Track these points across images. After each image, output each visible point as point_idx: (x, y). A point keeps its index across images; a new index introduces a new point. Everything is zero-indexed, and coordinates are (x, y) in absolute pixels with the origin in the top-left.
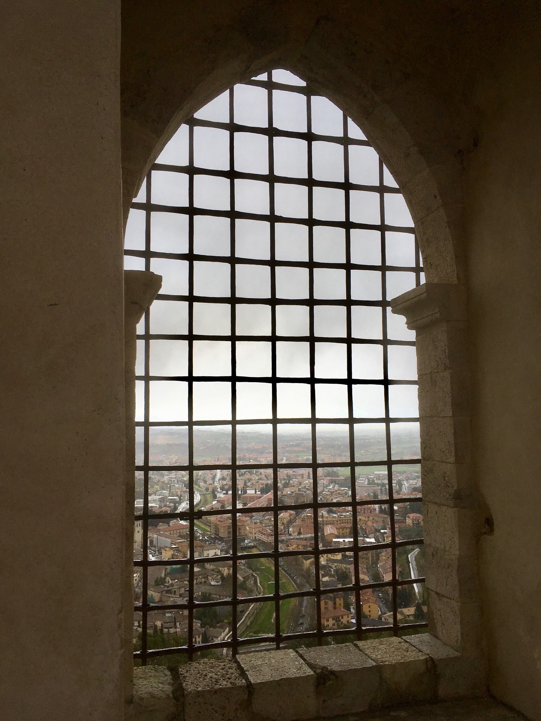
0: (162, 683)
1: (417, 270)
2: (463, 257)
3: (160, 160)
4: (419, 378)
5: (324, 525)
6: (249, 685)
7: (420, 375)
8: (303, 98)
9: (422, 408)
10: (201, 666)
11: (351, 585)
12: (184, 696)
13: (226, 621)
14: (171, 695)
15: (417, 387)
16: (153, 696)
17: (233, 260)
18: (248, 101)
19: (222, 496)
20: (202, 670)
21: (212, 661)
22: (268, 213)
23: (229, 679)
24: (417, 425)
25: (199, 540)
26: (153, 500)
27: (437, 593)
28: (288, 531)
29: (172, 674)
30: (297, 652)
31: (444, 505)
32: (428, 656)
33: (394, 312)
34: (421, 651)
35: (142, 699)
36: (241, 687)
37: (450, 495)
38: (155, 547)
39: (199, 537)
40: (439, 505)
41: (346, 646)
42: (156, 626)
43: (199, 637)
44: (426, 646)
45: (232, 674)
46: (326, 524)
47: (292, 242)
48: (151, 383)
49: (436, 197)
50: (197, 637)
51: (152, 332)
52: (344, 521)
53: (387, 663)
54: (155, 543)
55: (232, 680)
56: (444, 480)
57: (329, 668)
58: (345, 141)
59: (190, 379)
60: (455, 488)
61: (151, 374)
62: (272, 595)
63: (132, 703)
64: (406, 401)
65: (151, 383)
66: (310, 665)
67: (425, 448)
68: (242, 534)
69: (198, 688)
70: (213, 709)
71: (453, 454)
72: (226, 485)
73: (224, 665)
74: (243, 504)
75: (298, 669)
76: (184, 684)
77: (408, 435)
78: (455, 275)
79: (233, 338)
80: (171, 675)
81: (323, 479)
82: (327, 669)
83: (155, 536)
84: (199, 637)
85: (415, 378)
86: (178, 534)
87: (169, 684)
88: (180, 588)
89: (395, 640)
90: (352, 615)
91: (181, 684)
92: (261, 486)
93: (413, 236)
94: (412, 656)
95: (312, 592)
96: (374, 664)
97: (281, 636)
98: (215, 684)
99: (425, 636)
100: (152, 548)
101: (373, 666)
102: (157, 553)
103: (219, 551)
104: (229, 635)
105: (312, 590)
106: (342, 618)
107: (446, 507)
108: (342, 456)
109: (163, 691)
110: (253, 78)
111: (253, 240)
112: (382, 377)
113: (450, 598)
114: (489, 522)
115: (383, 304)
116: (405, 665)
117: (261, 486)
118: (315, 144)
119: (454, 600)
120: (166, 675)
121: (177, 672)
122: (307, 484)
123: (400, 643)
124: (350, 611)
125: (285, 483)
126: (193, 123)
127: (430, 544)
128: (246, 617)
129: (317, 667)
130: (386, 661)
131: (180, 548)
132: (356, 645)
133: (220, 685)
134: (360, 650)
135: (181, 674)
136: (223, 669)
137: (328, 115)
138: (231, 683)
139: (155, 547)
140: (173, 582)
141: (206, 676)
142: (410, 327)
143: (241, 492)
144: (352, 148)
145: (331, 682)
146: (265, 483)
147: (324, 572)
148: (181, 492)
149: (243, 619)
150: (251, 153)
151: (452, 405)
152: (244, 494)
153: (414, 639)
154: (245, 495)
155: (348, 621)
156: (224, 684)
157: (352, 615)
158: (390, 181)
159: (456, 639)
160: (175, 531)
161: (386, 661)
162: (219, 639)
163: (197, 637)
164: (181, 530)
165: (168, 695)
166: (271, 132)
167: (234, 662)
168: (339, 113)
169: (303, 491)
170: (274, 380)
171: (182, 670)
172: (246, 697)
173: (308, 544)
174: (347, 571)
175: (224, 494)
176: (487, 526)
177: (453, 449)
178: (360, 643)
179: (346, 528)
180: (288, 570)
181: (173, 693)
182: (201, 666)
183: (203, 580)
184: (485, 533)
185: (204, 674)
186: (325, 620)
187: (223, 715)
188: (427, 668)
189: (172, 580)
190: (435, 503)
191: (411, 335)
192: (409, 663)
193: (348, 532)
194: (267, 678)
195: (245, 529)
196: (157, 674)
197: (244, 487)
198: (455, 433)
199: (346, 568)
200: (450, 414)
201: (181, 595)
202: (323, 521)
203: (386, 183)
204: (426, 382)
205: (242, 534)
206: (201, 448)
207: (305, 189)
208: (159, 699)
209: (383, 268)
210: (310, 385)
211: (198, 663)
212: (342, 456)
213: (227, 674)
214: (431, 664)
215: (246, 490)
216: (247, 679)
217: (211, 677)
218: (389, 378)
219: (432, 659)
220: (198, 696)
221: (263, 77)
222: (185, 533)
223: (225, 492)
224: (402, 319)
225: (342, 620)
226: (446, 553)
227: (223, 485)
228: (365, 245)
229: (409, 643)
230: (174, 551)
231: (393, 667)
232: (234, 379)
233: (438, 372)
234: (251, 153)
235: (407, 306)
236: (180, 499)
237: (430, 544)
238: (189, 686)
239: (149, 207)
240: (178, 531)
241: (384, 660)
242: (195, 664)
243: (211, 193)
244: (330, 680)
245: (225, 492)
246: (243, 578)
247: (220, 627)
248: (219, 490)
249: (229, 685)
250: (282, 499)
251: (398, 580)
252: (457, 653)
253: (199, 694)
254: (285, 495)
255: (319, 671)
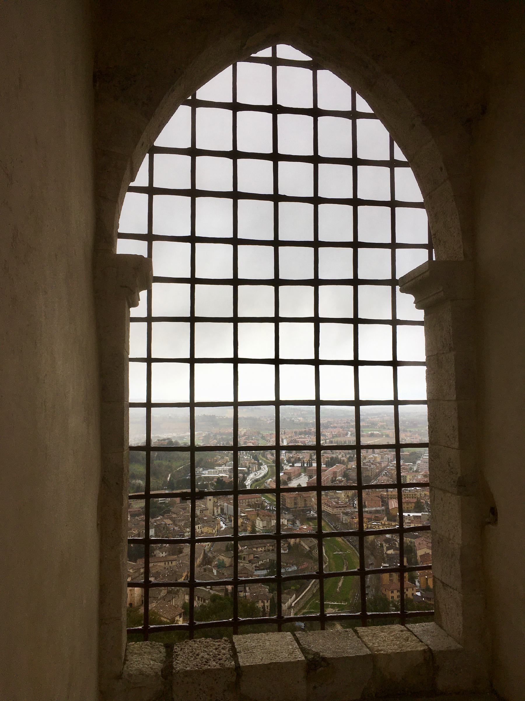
0: (155, 661)
1: (428, 247)
2: (470, 231)
3: (159, 142)
4: (427, 360)
5: (388, 498)
6: (238, 667)
7: (428, 357)
8: (309, 73)
9: (429, 392)
10: (196, 645)
11: (356, 570)
12: (172, 675)
13: (293, 588)
14: (160, 673)
15: (425, 368)
16: (141, 673)
17: (235, 241)
18: (252, 79)
19: (288, 468)
20: (195, 649)
21: (208, 640)
22: (272, 193)
23: (219, 660)
24: (424, 408)
25: (267, 509)
26: (224, 471)
27: (443, 583)
28: (353, 504)
29: (167, 652)
30: (294, 635)
31: (448, 492)
32: (426, 647)
33: (402, 291)
34: (421, 642)
35: (130, 676)
36: (229, 669)
37: (454, 482)
38: (225, 514)
39: (267, 506)
40: (445, 491)
41: (346, 631)
42: (227, 590)
43: (267, 602)
44: (428, 636)
45: (224, 655)
46: (391, 498)
47: (336, 223)
48: (153, 364)
49: (441, 169)
50: (266, 601)
51: (154, 315)
52: (409, 496)
53: (382, 652)
54: (225, 510)
55: (221, 662)
56: (449, 465)
57: (321, 654)
58: (353, 115)
59: (192, 361)
60: (459, 475)
61: (153, 356)
62: (273, 577)
63: (121, 679)
64: (415, 384)
65: (153, 364)
66: (304, 651)
67: (432, 432)
68: (308, 506)
69: (186, 667)
70: (201, 689)
71: (457, 439)
72: (292, 457)
73: (219, 645)
74: (309, 476)
75: (290, 654)
76: (174, 663)
77: (417, 420)
78: (462, 252)
79: (236, 320)
80: (166, 652)
81: (388, 454)
82: (319, 655)
83: (226, 504)
84: (267, 602)
85: (423, 359)
86: (247, 504)
87: (161, 662)
88: (249, 555)
89: (397, 627)
90: (417, 588)
91: (172, 662)
92: (326, 459)
93: (424, 211)
94: (413, 646)
95: (315, 575)
96: (369, 653)
97: (283, 617)
98: (205, 665)
99: (430, 625)
100: (223, 516)
101: (367, 655)
102: (228, 521)
103: (286, 521)
104: (296, 601)
105: (315, 573)
106: (407, 590)
107: (450, 494)
108: (406, 431)
109: (152, 668)
110: (253, 55)
111: (296, 222)
112: (390, 359)
113: (453, 588)
114: (493, 511)
115: (392, 282)
116: (402, 656)
117: (326, 459)
118: (321, 120)
119: (456, 590)
120: (160, 652)
121: (172, 649)
122: (372, 458)
123: (402, 631)
124: (415, 584)
125: (350, 457)
126: (195, 104)
127: (436, 531)
128: (312, 585)
129: (310, 652)
130: (381, 650)
131: (249, 517)
132: (356, 632)
133: (209, 666)
134: (359, 637)
135: (175, 652)
136: (216, 649)
137: (335, 91)
138: (220, 664)
139: (225, 514)
140: (243, 548)
141: (198, 655)
142: (418, 307)
143: (307, 465)
144: (360, 122)
145: (322, 668)
146: (330, 456)
147: (389, 544)
148: (249, 463)
149: (309, 587)
150: (255, 132)
151: (456, 388)
152: (309, 467)
153: (417, 628)
154: (311, 468)
155: (413, 594)
156: (214, 664)
157: (417, 588)
158: (399, 155)
159: (459, 630)
160: (244, 501)
161: (381, 650)
162: (286, 604)
163: (266, 601)
164: (250, 500)
165: (157, 673)
166: (275, 109)
167: (229, 642)
168: (348, 89)
169: (367, 465)
170: (277, 362)
171: (177, 648)
172: (234, 679)
173: (373, 517)
174: (412, 545)
175: (290, 466)
176: (491, 516)
177: (457, 433)
178: (361, 630)
179: (411, 503)
180: (353, 541)
181: (162, 672)
182: (196, 645)
183: (271, 548)
184: (490, 523)
185: (197, 653)
186: (390, 592)
187: (211, 695)
188: (425, 659)
189: (242, 546)
190: (441, 489)
191: (420, 315)
192: (406, 653)
193: (413, 507)
194: (258, 661)
195: (311, 501)
196: (152, 651)
197: (309, 460)
198: (459, 418)
199: (411, 542)
200: (454, 398)
201: (250, 561)
202: (388, 495)
203: (396, 158)
204: (434, 363)
205: (308, 506)
206: (268, 422)
207: (270, 163)
208: (147, 676)
209: (393, 246)
210: (314, 366)
211: (194, 641)
212: (406, 431)
213: (219, 655)
214: (429, 655)
215: (312, 463)
216: (237, 662)
217: (203, 657)
218: (398, 360)
219: (430, 650)
220: (186, 676)
221: (267, 53)
222: (253, 503)
223: (291, 464)
224: (410, 298)
225: (407, 593)
226: (450, 542)
227: (289, 458)
228: (374, 224)
229: (411, 631)
230: (243, 519)
231: (388, 656)
232: (236, 361)
233: (443, 353)
234: (255, 132)
235: (413, 283)
236: (248, 469)
237: (436, 531)
238: (179, 666)
239: (151, 191)
240: (247, 500)
241: (379, 648)
242: (191, 642)
243: (214, 174)
244: (321, 666)
245: (291, 464)
246: (310, 547)
247: (288, 594)
248: (285, 462)
249: (218, 666)
250: (347, 472)
251: (405, 566)
252: (459, 646)
253: (187, 674)
254: (350, 469)
255: (310, 657)
